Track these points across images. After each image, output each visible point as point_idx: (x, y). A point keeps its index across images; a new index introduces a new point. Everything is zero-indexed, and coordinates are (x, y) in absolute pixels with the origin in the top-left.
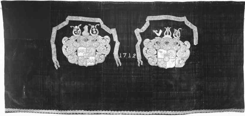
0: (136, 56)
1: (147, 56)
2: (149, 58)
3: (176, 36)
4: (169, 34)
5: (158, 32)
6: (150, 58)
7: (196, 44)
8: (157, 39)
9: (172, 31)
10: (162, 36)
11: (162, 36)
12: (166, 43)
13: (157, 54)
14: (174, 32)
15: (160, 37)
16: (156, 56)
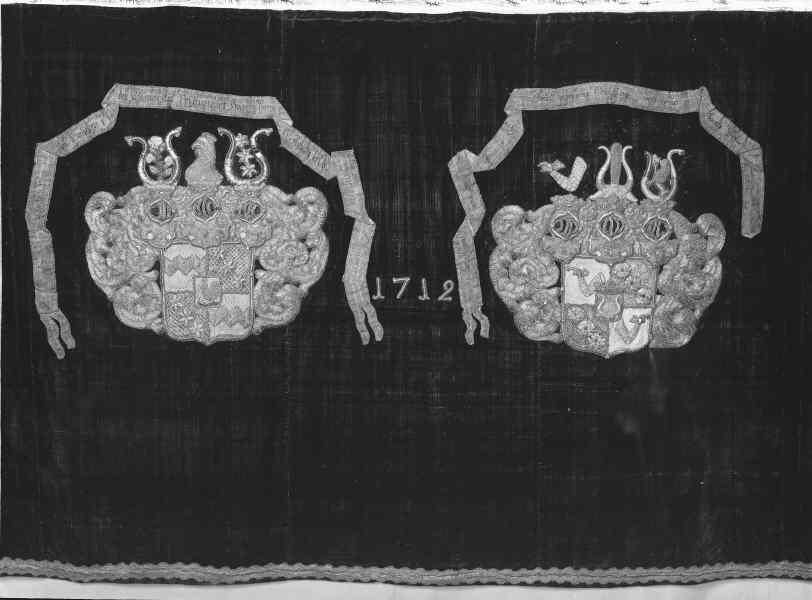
0: (455, 294)
3: (655, 191)
4: (623, 180)
5: (566, 172)
6: (524, 306)
10: (587, 188)
11: (587, 188)
13: (559, 284)
16: (554, 291)
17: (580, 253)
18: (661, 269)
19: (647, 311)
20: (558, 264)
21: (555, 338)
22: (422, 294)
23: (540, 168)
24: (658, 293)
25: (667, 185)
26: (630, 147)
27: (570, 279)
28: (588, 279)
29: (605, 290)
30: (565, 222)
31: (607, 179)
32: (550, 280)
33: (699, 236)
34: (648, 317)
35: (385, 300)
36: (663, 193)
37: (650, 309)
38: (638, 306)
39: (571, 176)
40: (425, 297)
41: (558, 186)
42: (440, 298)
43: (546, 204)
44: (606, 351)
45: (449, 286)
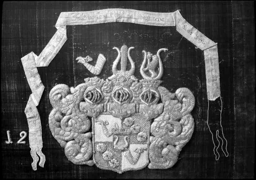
0: (27, 139)
1: (60, 134)
2: (67, 141)
3: (147, 72)
4: (128, 68)
5: (93, 63)
6: (69, 144)
7: (214, 96)
8: (90, 84)
9: (138, 59)
10: (106, 72)
11: (106, 72)
12: (119, 97)
13: (90, 130)
14: (142, 60)
15: (100, 76)
16: (87, 134)
17: (103, 111)
18: (152, 121)
19: (145, 146)
20: (90, 118)
21: (89, 163)
22: (7, 140)
23: (78, 61)
24: (151, 135)
25: (156, 70)
26: (132, 48)
27: (98, 127)
28: (109, 127)
29: (118, 134)
30: (92, 94)
31: (118, 67)
32: (85, 127)
33: (176, 101)
34: (146, 150)
35: (112, 45)
36: (152, 76)
37: (147, 145)
38: (139, 143)
39: (96, 66)
40: (9, 142)
41: (89, 72)
42: (19, 142)
43: (81, 83)
44: (120, 169)
45: (23, 135)
